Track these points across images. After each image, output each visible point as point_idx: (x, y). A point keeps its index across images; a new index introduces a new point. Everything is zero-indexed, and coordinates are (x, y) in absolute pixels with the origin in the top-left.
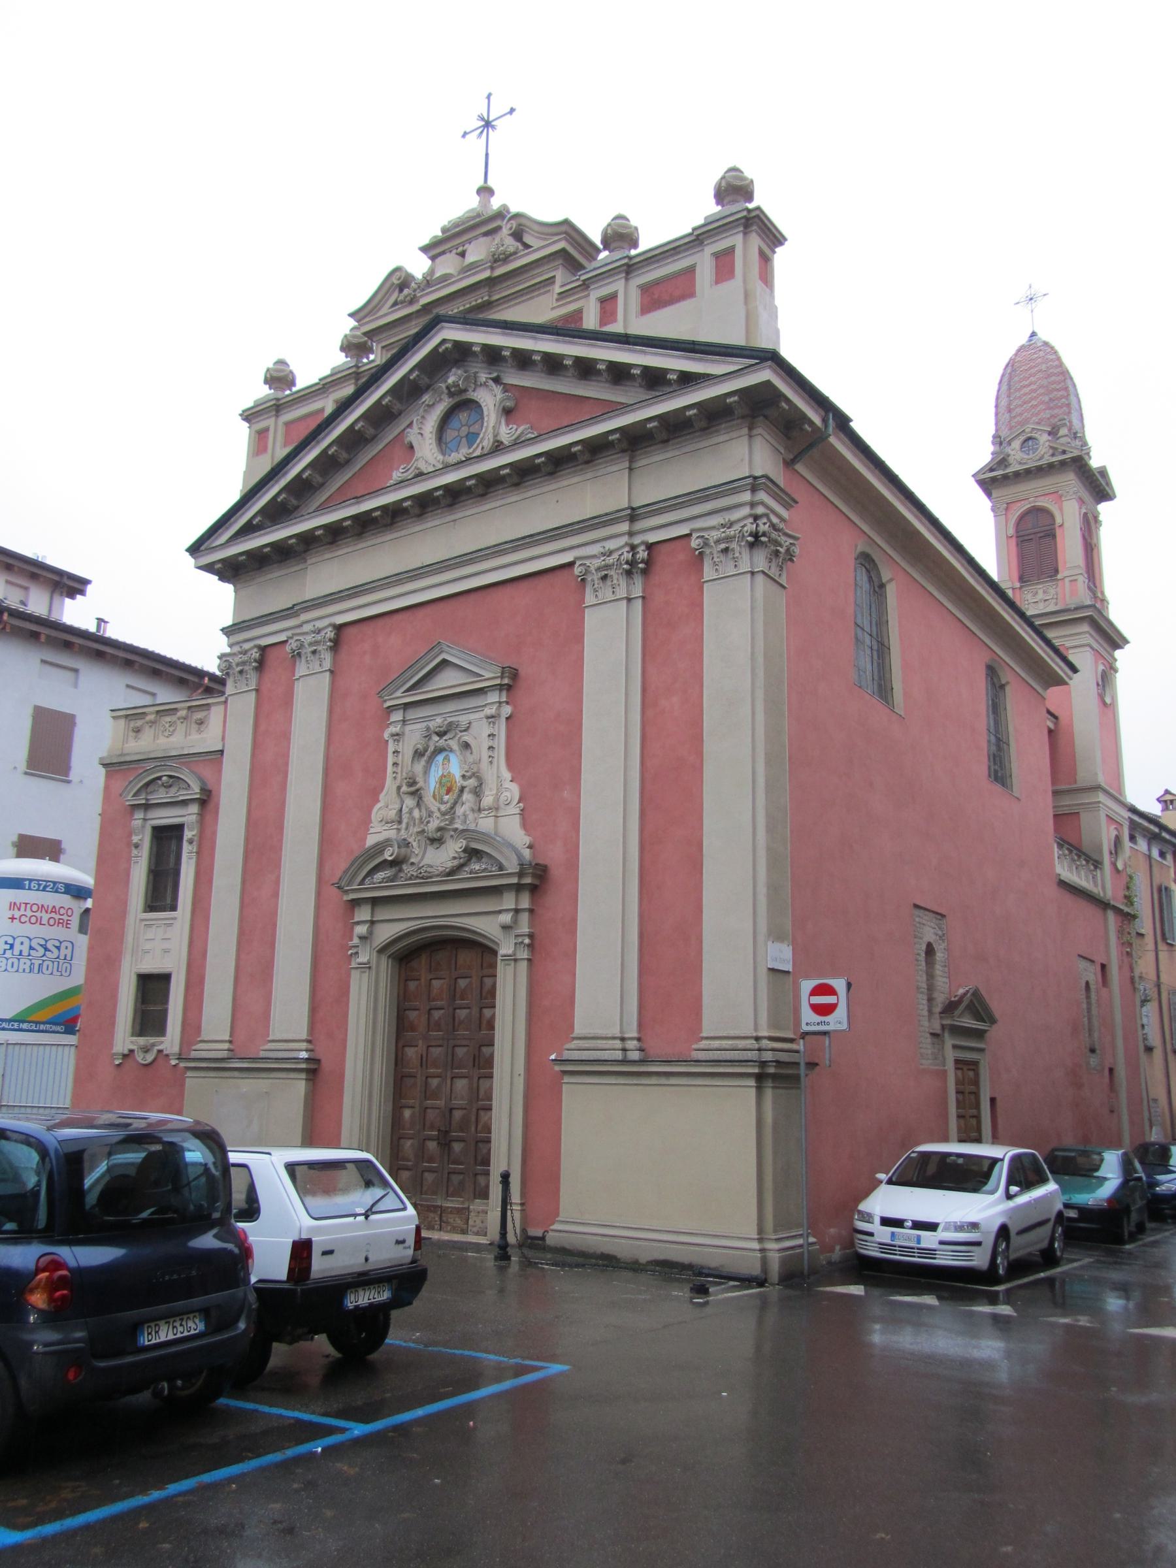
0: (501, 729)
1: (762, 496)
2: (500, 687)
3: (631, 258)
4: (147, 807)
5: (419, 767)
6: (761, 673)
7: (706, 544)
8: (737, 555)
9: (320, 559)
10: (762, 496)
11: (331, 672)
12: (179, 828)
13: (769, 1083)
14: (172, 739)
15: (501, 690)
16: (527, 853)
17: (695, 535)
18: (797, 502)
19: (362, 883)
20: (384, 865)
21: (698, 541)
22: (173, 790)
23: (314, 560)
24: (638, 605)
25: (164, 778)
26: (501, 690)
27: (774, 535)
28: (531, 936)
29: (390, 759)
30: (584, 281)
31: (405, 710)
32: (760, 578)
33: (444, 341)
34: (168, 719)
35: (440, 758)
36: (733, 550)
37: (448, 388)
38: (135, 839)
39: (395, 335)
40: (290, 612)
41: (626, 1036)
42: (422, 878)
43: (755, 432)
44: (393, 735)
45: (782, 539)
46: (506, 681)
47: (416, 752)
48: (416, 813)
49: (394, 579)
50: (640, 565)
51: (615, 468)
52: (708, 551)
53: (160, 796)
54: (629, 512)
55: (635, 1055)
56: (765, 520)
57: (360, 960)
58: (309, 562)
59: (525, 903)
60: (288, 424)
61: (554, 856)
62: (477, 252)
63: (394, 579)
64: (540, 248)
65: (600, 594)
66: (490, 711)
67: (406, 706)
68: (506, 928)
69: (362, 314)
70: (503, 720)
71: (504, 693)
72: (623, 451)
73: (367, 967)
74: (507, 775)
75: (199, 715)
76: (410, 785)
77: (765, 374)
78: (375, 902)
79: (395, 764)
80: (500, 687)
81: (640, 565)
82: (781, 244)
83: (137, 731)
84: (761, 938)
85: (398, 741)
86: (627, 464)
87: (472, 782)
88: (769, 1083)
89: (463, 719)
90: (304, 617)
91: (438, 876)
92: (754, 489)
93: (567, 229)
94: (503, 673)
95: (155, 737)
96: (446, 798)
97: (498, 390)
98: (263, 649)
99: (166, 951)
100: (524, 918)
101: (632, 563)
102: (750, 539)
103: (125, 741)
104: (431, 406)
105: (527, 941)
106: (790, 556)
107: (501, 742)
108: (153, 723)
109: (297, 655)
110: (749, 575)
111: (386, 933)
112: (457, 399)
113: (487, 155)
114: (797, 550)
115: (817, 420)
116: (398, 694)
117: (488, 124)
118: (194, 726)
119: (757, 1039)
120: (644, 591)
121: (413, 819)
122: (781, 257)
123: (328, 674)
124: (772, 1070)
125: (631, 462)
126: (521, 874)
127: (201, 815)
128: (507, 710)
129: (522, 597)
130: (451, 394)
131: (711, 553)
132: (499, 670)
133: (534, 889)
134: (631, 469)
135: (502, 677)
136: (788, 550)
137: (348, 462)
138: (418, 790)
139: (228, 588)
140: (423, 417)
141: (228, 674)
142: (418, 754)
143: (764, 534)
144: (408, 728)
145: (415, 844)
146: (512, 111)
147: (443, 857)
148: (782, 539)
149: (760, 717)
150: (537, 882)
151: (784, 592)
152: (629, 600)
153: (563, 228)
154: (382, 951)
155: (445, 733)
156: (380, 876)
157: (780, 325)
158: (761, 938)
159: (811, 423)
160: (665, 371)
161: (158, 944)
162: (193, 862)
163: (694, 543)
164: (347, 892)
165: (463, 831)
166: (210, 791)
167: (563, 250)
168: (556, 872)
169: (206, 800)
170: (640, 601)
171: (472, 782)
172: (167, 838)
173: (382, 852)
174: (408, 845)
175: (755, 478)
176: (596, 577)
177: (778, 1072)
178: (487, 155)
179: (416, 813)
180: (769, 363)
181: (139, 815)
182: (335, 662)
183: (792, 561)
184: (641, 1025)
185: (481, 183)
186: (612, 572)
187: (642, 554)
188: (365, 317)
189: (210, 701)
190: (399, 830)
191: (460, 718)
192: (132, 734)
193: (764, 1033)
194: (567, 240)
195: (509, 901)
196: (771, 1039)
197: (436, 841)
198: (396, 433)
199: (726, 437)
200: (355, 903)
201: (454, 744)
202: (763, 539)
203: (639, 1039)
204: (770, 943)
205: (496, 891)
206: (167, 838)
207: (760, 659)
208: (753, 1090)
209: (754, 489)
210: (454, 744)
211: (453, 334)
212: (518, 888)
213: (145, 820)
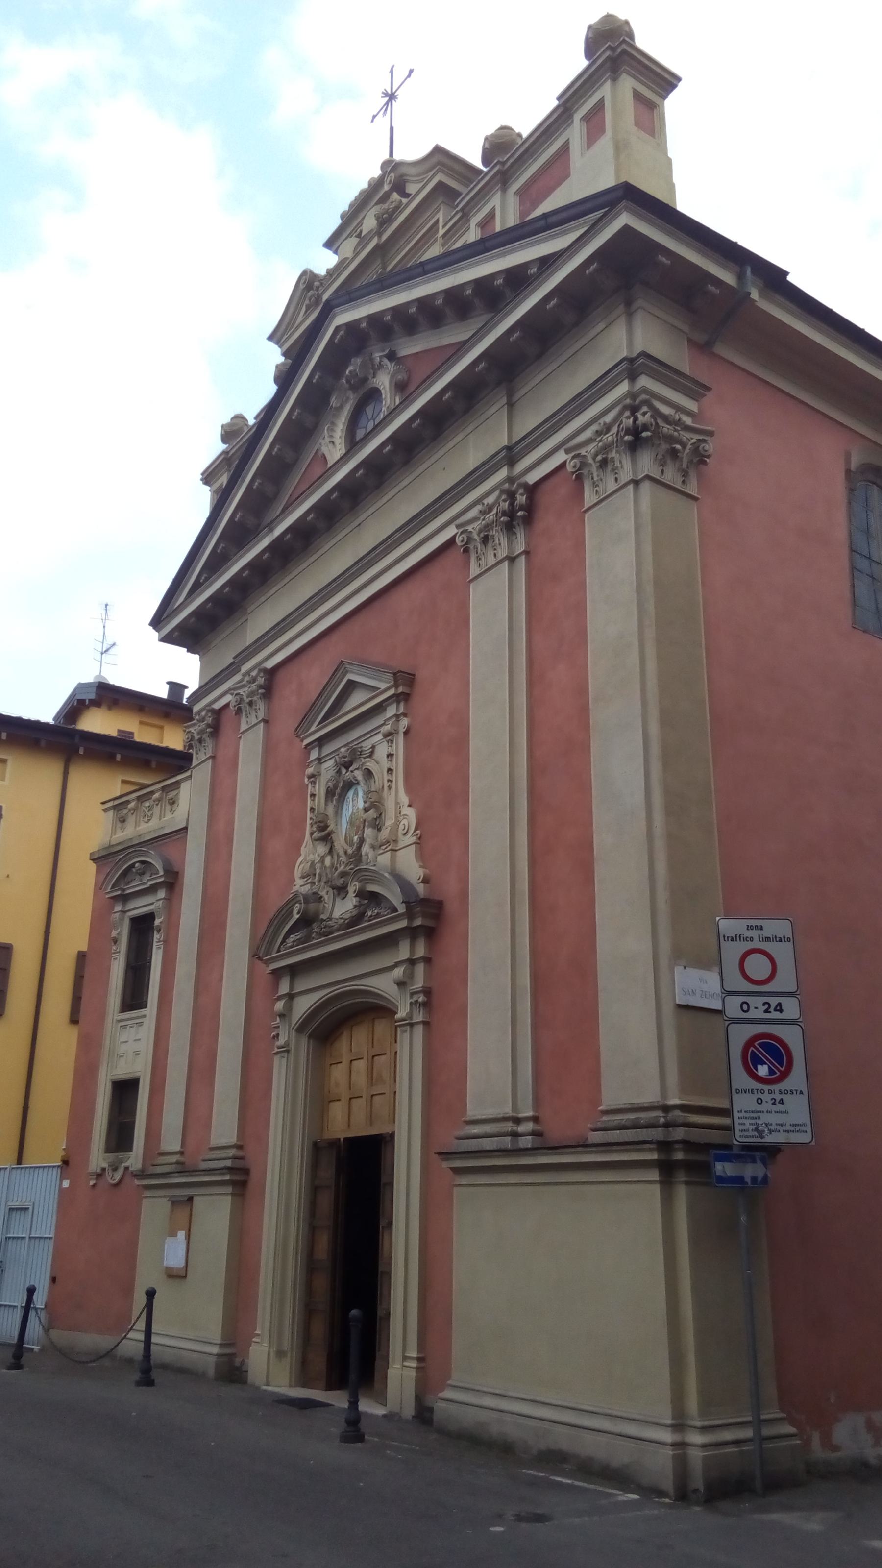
1: (644, 381)
2: (397, 698)
3: (503, 163)
4: (125, 898)
6: (651, 607)
8: (617, 464)
9: (257, 604)
10: (644, 381)
12: (151, 916)
13: (681, 1176)
14: (150, 824)
15: (398, 703)
16: (421, 889)
18: (708, 389)
19: (279, 951)
22: (146, 877)
23: (253, 607)
24: (522, 561)
25: (137, 865)
26: (398, 703)
27: (666, 429)
28: (427, 991)
30: (462, 209)
32: (646, 486)
33: (338, 329)
34: (147, 804)
36: (613, 459)
37: (348, 382)
38: (114, 933)
41: (520, 1115)
43: (635, 306)
44: (310, 777)
45: (685, 436)
46: (400, 690)
48: (328, 861)
50: (520, 513)
51: (493, 410)
53: (135, 886)
55: (526, 1142)
56: (645, 409)
58: (249, 610)
59: (421, 951)
61: (448, 889)
62: (370, 223)
64: (418, 191)
66: (387, 728)
68: (401, 984)
69: (279, 334)
70: (401, 735)
72: (498, 384)
73: (286, 1050)
74: (404, 799)
75: (172, 794)
77: (624, 219)
81: (520, 513)
82: (673, 87)
83: (123, 821)
84: (664, 962)
86: (504, 400)
87: (372, 814)
88: (681, 1176)
91: (338, 930)
92: (633, 377)
93: (440, 158)
94: (396, 681)
95: (137, 824)
97: (390, 366)
99: (137, 1054)
100: (420, 969)
101: (511, 514)
103: (114, 832)
105: (421, 998)
106: (700, 458)
108: (135, 809)
109: (239, 711)
110: (631, 487)
111: (303, 1005)
112: (362, 392)
113: (392, 129)
114: (709, 447)
115: (727, 277)
116: (313, 728)
117: (391, 97)
118: (168, 807)
119: (666, 1109)
120: (527, 544)
122: (674, 106)
124: (679, 1156)
125: (510, 395)
127: (168, 899)
128: (404, 722)
129: (416, 591)
130: (354, 388)
132: (390, 677)
134: (511, 405)
135: (396, 686)
136: (696, 450)
138: (329, 834)
139: (197, 657)
141: (191, 747)
143: (645, 427)
145: (326, 897)
146: (411, 71)
147: (343, 908)
148: (685, 436)
149: (651, 666)
150: (429, 923)
151: (694, 506)
152: (512, 559)
153: (434, 160)
156: (293, 938)
157: (675, 180)
158: (664, 962)
159: (718, 282)
160: (525, 266)
161: (130, 1047)
162: (161, 952)
163: (569, 468)
164: (267, 963)
166: (177, 874)
167: (440, 185)
168: (451, 908)
169: (172, 881)
170: (523, 557)
171: (372, 814)
172: (142, 927)
174: (320, 899)
177: (688, 1154)
178: (392, 129)
180: (624, 203)
181: (118, 908)
182: (269, 710)
183: (705, 463)
184: (537, 1101)
185: (386, 156)
186: (493, 532)
187: (521, 499)
188: (283, 336)
189: (179, 777)
190: (313, 883)
192: (119, 825)
193: (674, 1101)
194: (443, 172)
195: (404, 952)
196: (684, 1108)
197: (341, 891)
198: (314, 452)
199: (601, 326)
200: (277, 974)
201: (359, 775)
202: (644, 434)
203: (535, 1119)
204: (678, 970)
206: (142, 927)
207: (649, 589)
208: (657, 1188)
209: (633, 377)
211: (344, 317)
212: (412, 933)
213: (124, 912)
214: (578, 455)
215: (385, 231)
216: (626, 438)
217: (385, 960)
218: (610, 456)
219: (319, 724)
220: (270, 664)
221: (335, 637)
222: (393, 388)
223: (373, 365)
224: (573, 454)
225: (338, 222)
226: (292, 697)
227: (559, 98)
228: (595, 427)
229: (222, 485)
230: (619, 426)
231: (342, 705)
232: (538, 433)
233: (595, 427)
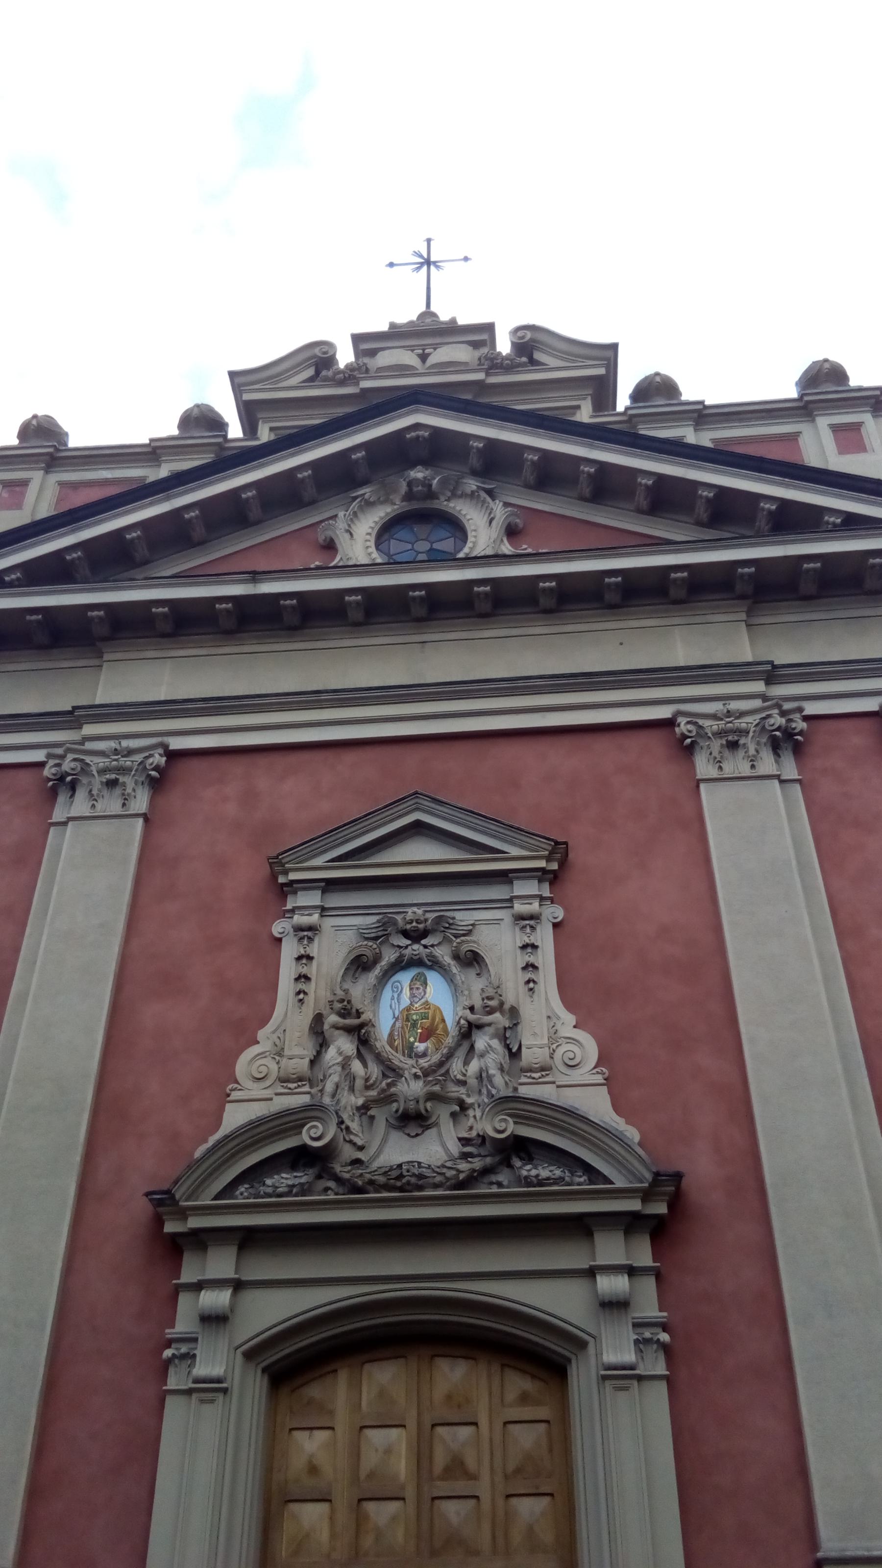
0: (545, 937)
5: (359, 990)
7: (85, 769)
11: (146, 818)
15: (540, 881)
17: (70, 756)
19: (229, 1189)
20: (301, 1157)
21: (73, 765)
29: (287, 969)
31: (324, 892)
35: (405, 978)
39: (288, 418)
40: (71, 718)
42: (401, 1189)
44: (298, 929)
47: (359, 957)
49: (274, 700)
52: (84, 780)
54: (769, 667)
57: (201, 1370)
60: (62, 484)
63: (274, 700)
65: (99, 806)
67: (330, 886)
71: (546, 886)
76: (344, 1013)
78: (249, 1240)
79: (303, 978)
80: (542, 875)
85: (311, 940)
89: (464, 918)
90: (89, 730)
96: (421, 1047)
98: (173, 756)
100: (649, 1285)
102: (154, 773)
104: (368, 504)
107: (546, 958)
111: (269, 1311)
112: (415, 505)
116: (319, 861)
121: (351, 1078)
123: (140, 821)
126: (647, 1196)
129: (560, 757)
131: (90, 783)
133: (659, 1231)
137: (202, 543)
138: (362, 1026)
140: (355, 514)
142: (359, 964)
144: (328, 923)
154: (250, 1355)
155: (425, 934)
156: (284, 1180)
163: (47, 772)
165: (507, 1099)
173: (298, 1128)
175: (775, 667)
176: (97, 781)
179: (357, 1066)
191: (459, 916)
197: (413, 1120)
205: (581, 1227)
210: (443, 954)
212: (630, 1224)
214: (695, 724)
215: (496, 374)
216: (153, 773)
217: (568, 1255)
218: (742, 742)
219: (332, 860)
220: (177, 744)
221: (566, 742)
222: (504, 527)
223: (455, 488)
224: (689, 719)
225: (385, 328)
226: (210, 807)
227: (151, 440)
228: (113, 744)
229: (145, 478)
230: (147, 758)
231: (373, 854)
232: (521, 684)
233: (113, 744)
